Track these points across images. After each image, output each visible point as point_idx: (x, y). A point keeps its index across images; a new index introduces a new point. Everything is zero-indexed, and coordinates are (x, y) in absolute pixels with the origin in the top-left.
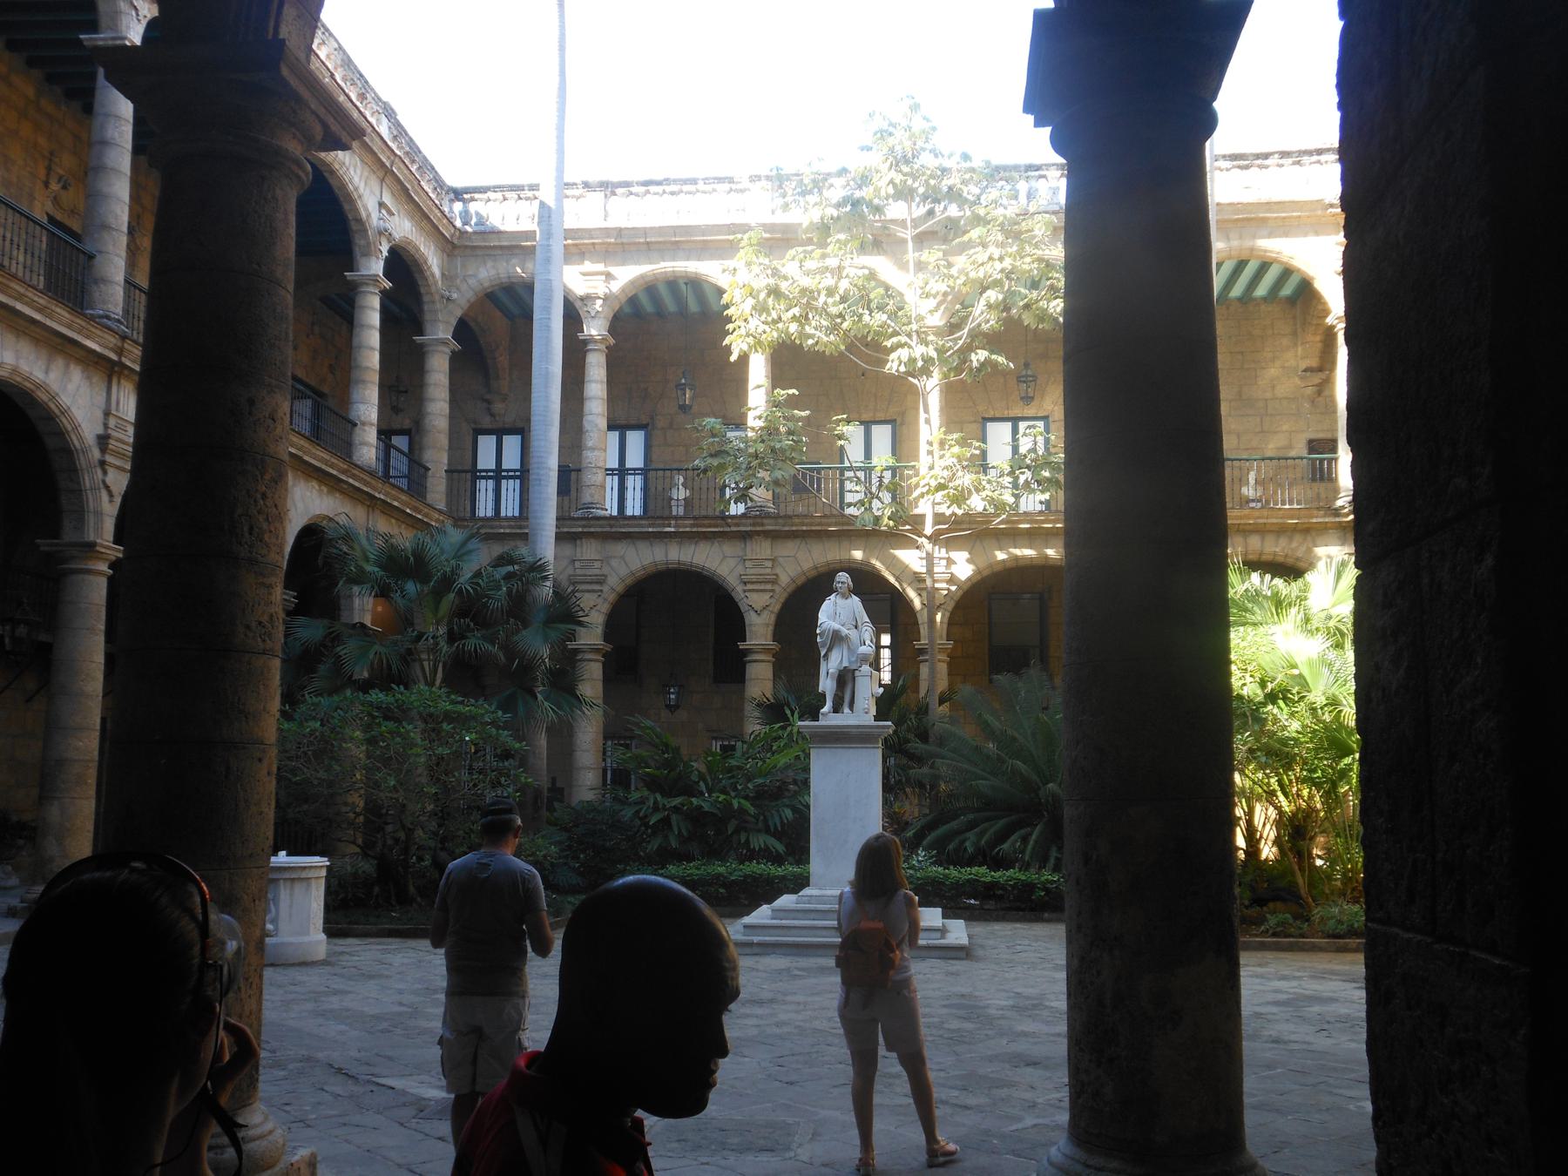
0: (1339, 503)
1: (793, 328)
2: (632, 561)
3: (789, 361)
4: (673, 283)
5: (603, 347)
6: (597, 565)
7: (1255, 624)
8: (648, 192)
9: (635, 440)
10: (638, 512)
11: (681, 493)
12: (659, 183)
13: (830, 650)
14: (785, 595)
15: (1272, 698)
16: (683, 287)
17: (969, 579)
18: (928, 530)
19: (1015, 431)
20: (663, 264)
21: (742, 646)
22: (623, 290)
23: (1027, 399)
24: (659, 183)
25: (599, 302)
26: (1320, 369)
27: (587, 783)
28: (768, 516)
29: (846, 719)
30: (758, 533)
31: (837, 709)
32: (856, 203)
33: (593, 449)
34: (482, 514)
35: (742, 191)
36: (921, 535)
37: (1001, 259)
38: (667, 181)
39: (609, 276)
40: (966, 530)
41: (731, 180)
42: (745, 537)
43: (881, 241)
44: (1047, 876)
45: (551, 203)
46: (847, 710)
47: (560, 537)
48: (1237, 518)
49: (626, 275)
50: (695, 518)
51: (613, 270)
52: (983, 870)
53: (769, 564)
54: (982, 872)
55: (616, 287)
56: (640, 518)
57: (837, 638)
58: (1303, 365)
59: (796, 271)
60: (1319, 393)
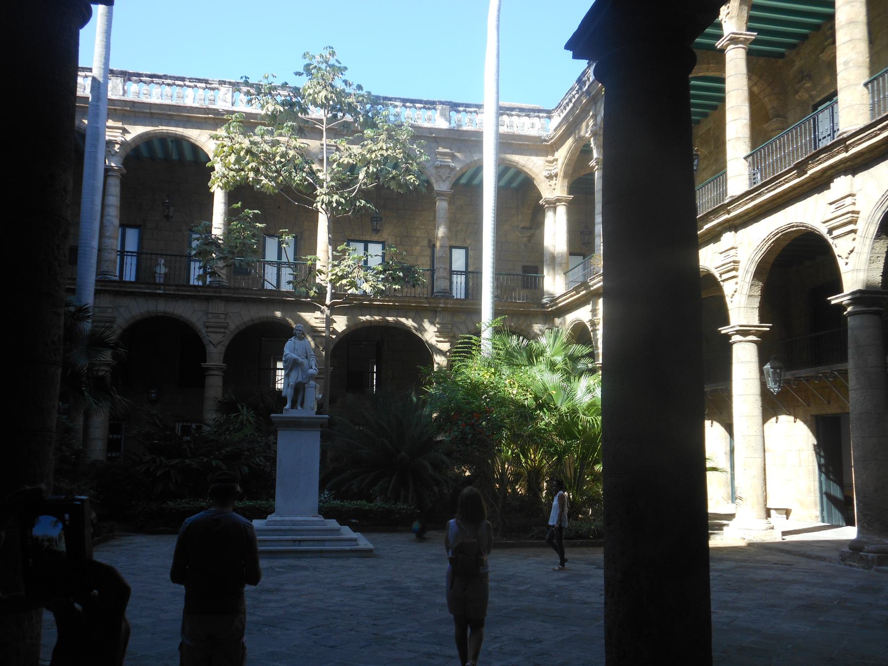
0: (544, 301)
1: (251, 175)
2: (134, 309)
3: (239, 193)
4: (163, 139)
5: (119, 174)
6: (110, 310)
7: (517, 365)
8: (152, 82)
9: (132, 236)
10: (133, 279)
11: (162, 270)
12: (159, 77)
14: (232, 336)
15: (540, 407)
16: (170, 144)
17: (343, 331)
18: (328, 302)
19: (366, 249)
20: (161, 128)
21: (204, 365)
22: (134, 140)
23: (377, 231)
24: (159, 77)
25: (117, 146)
26: (530, 228)
27: (98, 450)
28: (224, 287)
29: (298, 413)
30: (217, 297)
32: (292, 105)
33: (110, 238)
34: (127, 279)
35: (213, 89)
36: (324, 304)
37: (387, 150)
38: (165, 77)
39: (125, 131)
40: (348, 304)
41: (206, 82)
42: (208, 299)
43: (306, 129)
44: (400, 505)
45: (101, 80)
46: (299, 408)
47: (97, 292)
49: (136, 131)
50: (177, 286)
51: (127, 127)
52: (364, 502)
53: (223, 316)
54: (363, 503)
55: (129, 137)
58: (522, 225)
59: (261, 139)
60: (529, 241)
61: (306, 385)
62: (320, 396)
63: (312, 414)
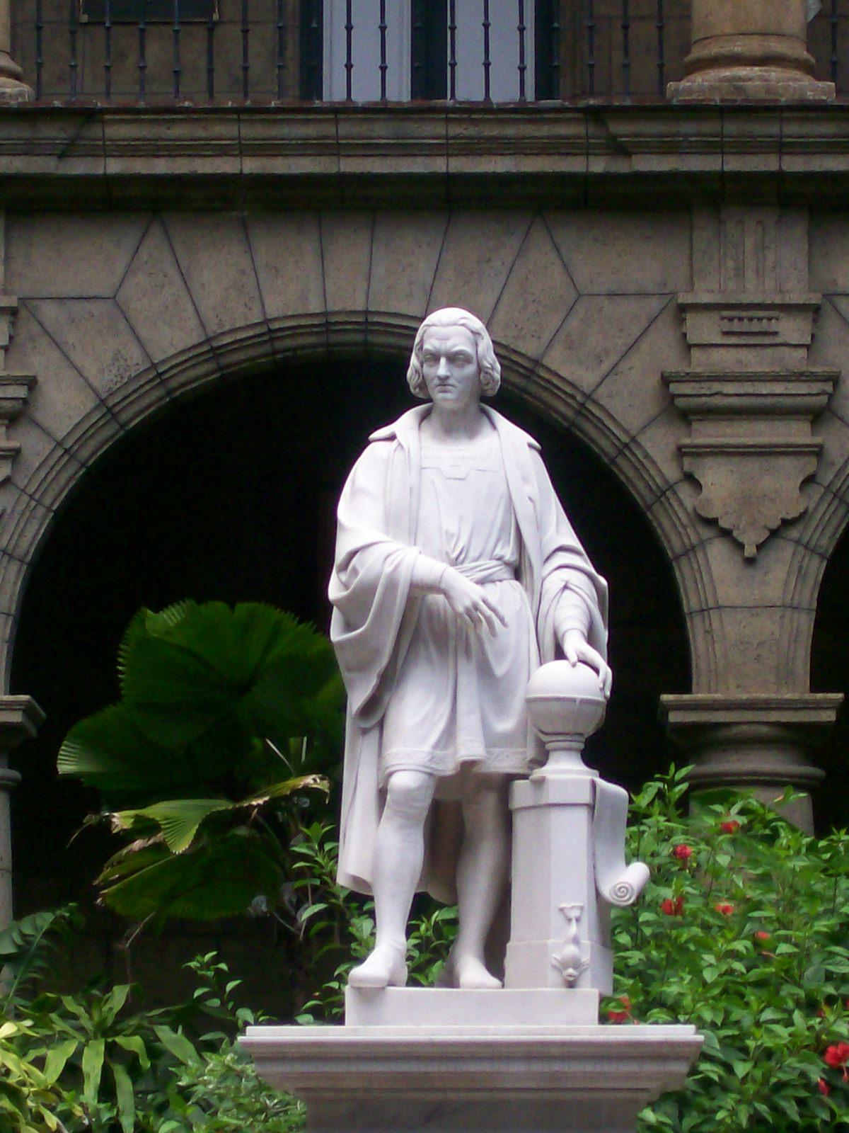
10: (506, 90)
13: (389, 681)
31: (430, 959)
46: (472, 969)
48: (180, 616)
56: (518, 111)
57: (430, 630)
61: (521, 793)
62: (636, 874)
63: (574, 1018)
